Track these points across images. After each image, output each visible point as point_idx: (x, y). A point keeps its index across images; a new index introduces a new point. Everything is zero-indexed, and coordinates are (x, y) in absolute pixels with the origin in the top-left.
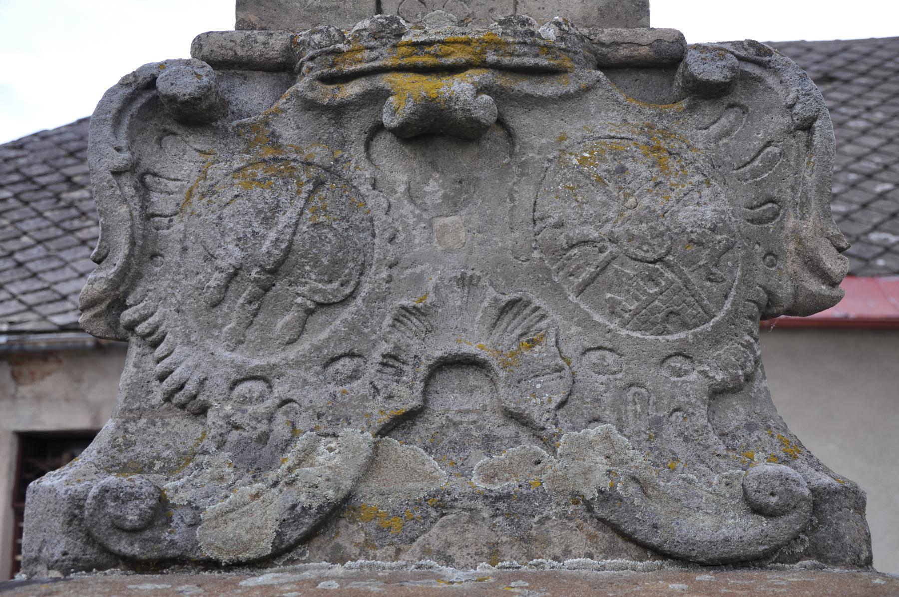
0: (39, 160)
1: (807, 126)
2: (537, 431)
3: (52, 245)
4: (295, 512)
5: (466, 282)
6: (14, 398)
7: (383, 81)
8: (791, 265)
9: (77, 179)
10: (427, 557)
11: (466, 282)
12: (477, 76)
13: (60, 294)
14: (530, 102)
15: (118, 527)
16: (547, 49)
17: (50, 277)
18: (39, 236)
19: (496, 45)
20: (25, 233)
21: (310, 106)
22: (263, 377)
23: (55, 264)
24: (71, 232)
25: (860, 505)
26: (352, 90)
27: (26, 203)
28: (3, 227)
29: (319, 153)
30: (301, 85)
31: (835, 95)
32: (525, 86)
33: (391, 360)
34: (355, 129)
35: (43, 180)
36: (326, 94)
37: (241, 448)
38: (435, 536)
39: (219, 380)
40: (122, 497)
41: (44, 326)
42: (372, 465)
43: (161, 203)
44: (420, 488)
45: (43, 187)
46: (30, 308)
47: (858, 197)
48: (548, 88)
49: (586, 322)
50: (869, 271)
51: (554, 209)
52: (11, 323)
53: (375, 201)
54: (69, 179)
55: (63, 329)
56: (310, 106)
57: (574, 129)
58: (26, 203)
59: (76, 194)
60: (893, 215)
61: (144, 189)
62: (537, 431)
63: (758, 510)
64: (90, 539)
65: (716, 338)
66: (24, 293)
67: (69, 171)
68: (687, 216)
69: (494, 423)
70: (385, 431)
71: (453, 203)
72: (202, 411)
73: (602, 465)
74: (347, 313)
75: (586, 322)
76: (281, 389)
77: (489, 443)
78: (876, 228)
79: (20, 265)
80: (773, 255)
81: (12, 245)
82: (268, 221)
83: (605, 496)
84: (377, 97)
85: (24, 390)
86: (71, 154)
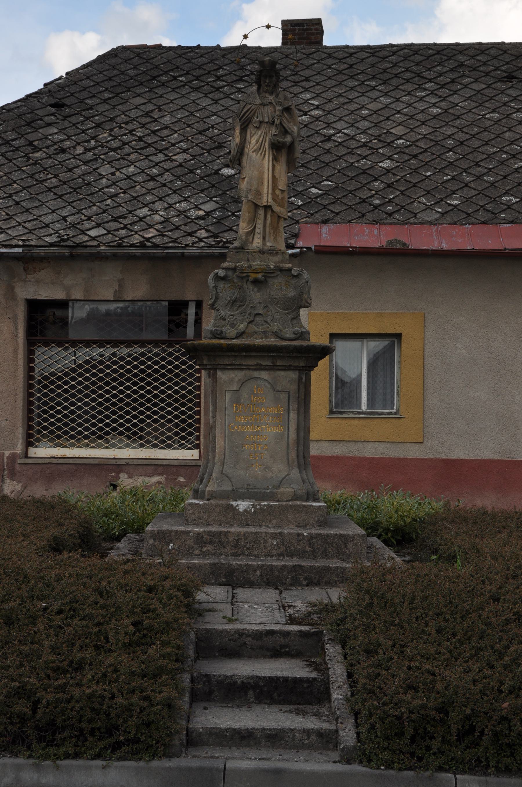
0: (10, 128)
1: (307, 282)
2: (268, 324)
3: (32, 190)
4: (238, 333)
5: (260, 303)
6: (25, 281)
7: (249, 274)
8: (304, 302)
9: (36, 143)
10: (235, 525)
11: (260, 303)
12: (262, 274)
13: (44, 223)
14: (270, 277)
15: (217, 334)
16: (272, 269)
17: (35, 212)
18: (24, 184)
19: (265, 269)
20: (15, 182)
21: (238, 277)
22: (233, 315)
23: (37, 204)
24: (41, 182)
25: (309, 333)
26: (245, 275)
27: (10, 161)
28: (1, 177)
29: (240, 284)
30: (237, 273)
31: (511, 92)
32: (269, 275)
33: (250, 314)
34: (245, 280)
35: (15, 143)
36: (241, 275)
37: (230, 325)
38: (255, 336)
39: (227, 316)
40: (217, 330)
41: (41, 243)
42: (247, 328)
43: (219, 291)
44: (253, 330)
45: (17, 149)
46: (30, 232)
47: (503, 171)
48: (272, 275)
49: (276, 309)
50: (496, 221)
51: (272, 293)
52: (23, 240)
53: (248, 291)
54: (31, 143)
55: (52, 245)
56: (238, 277)
57: (275, 281)
58: (10, 161)
59: (38, 155)
60: (519, 184)
61: (216, 289)
62: (268, 324)
63: (295, 334)
64: (213, 335)
65: (293, 312)
66: (25, 222)
67: (31, 137)
68: (290, 295)
69: (263, 322)
70: (249, 323)
71: (258, 292)
72: (225, 320)
73: (276, 328)
74: (244, 307)
75: (276, 309)
76: (235, 317)
77: (262, 325)
78: (507, 193)
79: (17, 203)
80: (302, 300)
81: (8, 189)
82: (234, 294)
83: (276, 332)
84: (248, 276)
85: (29, 277)
86: (29, 124)
